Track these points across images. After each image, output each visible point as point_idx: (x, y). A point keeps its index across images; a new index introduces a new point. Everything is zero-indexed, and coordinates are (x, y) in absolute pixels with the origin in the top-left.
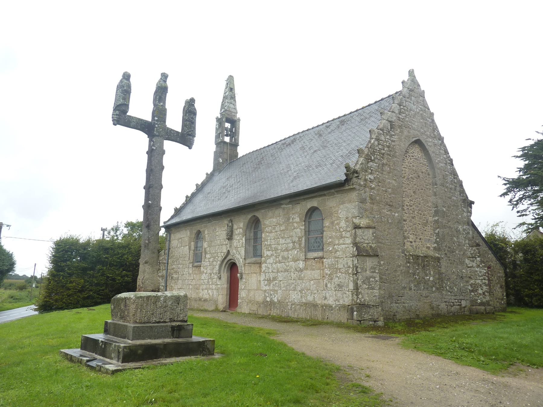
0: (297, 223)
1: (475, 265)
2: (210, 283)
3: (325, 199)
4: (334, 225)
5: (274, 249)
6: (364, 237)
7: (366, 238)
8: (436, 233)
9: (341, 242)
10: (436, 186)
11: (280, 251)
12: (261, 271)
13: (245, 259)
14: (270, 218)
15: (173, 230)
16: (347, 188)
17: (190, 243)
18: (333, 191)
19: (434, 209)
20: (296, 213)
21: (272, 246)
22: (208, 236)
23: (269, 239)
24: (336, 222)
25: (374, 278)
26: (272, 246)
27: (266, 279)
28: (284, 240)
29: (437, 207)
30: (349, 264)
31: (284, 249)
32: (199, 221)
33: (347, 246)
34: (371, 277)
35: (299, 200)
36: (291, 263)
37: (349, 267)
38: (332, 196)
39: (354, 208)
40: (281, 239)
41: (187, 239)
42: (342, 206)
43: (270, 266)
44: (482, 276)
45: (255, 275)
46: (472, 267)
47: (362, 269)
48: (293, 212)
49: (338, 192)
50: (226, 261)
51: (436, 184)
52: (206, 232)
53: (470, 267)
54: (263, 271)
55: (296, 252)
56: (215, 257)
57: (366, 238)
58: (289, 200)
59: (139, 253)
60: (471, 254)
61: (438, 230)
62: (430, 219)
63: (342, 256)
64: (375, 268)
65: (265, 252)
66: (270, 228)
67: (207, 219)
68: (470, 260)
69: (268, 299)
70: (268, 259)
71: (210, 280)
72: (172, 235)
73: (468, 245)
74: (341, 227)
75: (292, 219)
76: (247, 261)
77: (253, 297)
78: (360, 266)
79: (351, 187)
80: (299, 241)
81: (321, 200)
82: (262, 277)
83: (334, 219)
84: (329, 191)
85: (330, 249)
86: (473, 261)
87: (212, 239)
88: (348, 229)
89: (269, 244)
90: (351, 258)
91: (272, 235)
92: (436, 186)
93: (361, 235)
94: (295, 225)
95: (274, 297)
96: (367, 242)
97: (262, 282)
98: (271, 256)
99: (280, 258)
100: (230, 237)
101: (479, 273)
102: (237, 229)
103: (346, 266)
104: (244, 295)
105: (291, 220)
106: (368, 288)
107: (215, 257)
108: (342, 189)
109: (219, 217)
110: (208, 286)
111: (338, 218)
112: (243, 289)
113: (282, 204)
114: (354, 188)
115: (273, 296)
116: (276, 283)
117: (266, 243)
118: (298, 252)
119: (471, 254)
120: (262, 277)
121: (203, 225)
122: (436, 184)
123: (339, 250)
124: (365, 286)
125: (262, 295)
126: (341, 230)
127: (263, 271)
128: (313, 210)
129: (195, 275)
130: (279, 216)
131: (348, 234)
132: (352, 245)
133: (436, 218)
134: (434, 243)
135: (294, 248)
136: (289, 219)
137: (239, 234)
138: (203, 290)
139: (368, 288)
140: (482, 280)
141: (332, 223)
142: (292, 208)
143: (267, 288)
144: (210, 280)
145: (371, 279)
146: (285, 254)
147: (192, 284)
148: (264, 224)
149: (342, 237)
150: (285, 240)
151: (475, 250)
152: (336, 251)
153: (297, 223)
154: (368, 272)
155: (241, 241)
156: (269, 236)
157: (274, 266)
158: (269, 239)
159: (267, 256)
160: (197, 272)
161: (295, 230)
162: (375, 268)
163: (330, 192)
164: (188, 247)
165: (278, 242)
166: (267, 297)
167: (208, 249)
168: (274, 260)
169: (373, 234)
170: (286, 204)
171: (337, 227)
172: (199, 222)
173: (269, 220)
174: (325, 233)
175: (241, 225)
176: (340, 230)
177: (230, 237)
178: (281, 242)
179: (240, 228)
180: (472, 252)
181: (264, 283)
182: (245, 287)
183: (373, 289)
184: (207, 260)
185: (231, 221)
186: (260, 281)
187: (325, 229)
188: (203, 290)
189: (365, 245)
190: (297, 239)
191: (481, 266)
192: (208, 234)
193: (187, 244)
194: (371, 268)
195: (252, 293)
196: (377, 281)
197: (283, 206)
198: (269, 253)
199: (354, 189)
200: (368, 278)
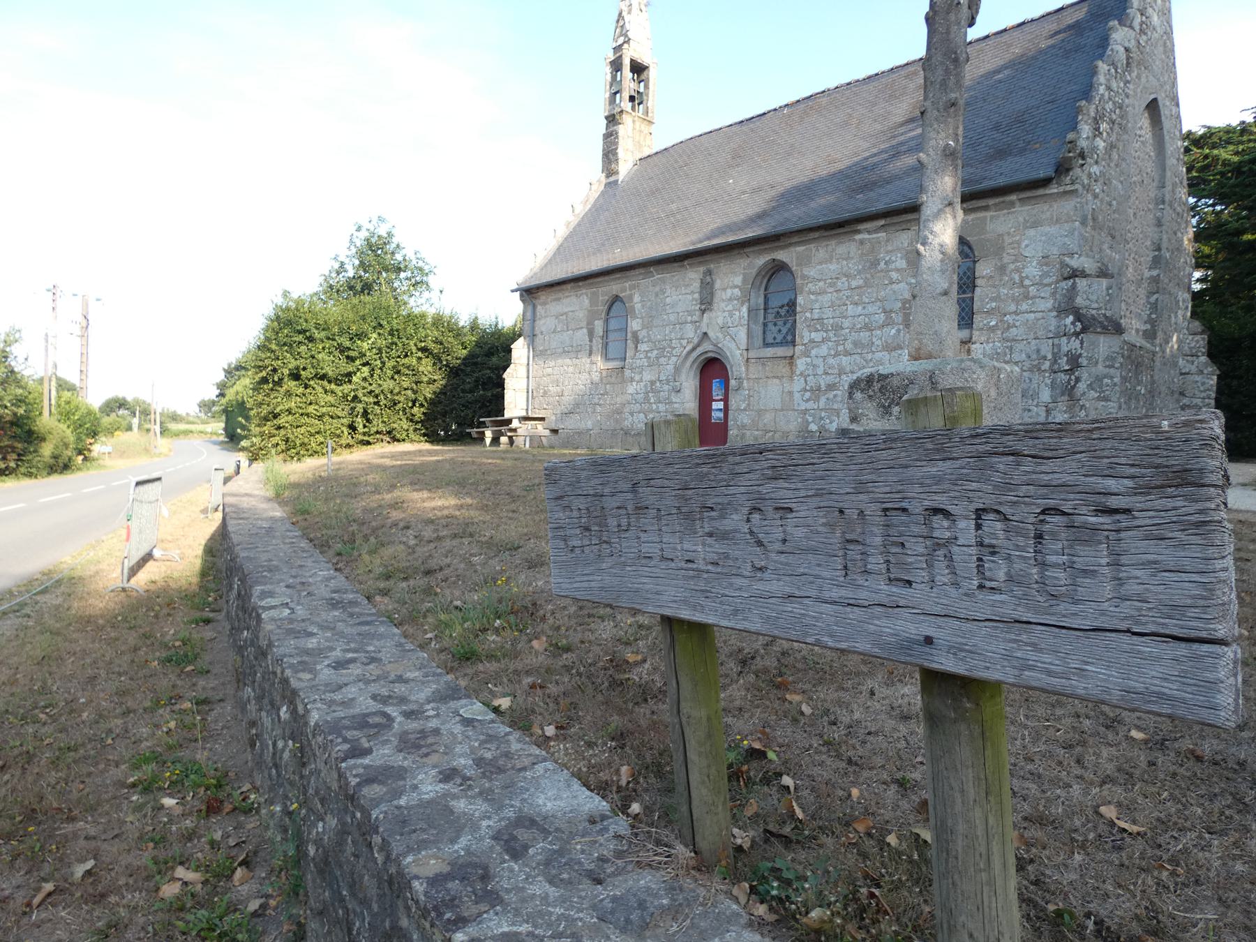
0: (898, 270)
1: (1193, 368)
2: (652, 401)
3: (986, 217)
4: (1008, 272)
5: (832, 326)
6: (1090, 297)
7: (1094, 298)
8: (1150, 303)
9: (1024, 307)
10: (1162, 206)
11: (847, 331)
12: (793, 372)
13: (747, 350)
14: (821, 263)
15: (543, 296)
16: (1056, 191)
17: (590, 324)
18: (1013, 197)
19: (1152, 254)
20: (898, 249)
21: (825, 321)
22: (643, 306)
23: (817, 306)
24: (1012, 266)
25: (1112, 378)
26: (825, 321)
27: (808, 388)
28: (860, 308)
29: (1159, 249)
30: (1043, 353)
31: (859, 326)
32: (618, 276)
33: (1039, 315)
34: (1106, 376)
35: (909, 221)
36: (880, 354)
37: (1045, 358)
38: (1005, 211)
39: (1066, 236)
40: (850, 307)
41: (581, 314)
42: (1032, 232)
43: (819, 362)
44: (1205, 391)
45: (777, 381)
46: (1188, 374)
47: (1090, 359)
48: (890, 248)
49: (998, 207)
50: (695, 354)
51: (1163, 202)
52: (637, 298)
53: (1185, 374)
54: (798, 373)
55: (893, 331)
56: (664, 348)
57: (1094, 298)
58: (882, 222)
59: (268, 381)
60: (1191, 348)
61: (1155, 296)
62: (1147, 274)
63: (1025, 337)
64: (1113, 359)
65: (806, 334)
66: (821, 284)
67: (642, 271)
68: (1187, 361)
69: (813, 427)
70: (813, 348)
71: (650, 395)
72: (539, 307)
73: (1186, 331)
74: (1027, 277)
75: (886, 263)
76: (752, 354)
77: (773, 424)
78: (1085, 354)
79: (1069, 188)
80: (904, 308)
81: (973, 220)
82: (798, 384)
83: (1006, 259)
84: (1001, 199)
85: (993, 323)
86: (1193, 363)
87: (654, 313)
88: (1046, 281)
89: (816, 317)
90: (1051, 341)
91: (826, 299)
92: (1162, 206)
93: (1085, 292)
94: (894, 275)
95: (831, 423)
96: (1095, 305)
97: (797, 396)
98: (823, 341)
99: (849, 346)
100: (706, 303)
101: (1199, 384)
102: (724, 289)
103: (1034, 356)
104: (745, 421)
105: (882, 264)
106: (1099, 399)
107: (664, 348)
108: (1041, 192)
109: (676, 265)
110: (646, 407)
111: (1019, 257)
112: (745, 410)
113: (859, 232)
114: (1074, 192)
115: (828, 421)
116: (835, 396)
117: (808, 315)
118: (899, 331)
119: (1191, 348)
120: (798, 384)
121: (627, 285)
122: (1163, 202)
123: (1018, 324)
124: (1093, 394)
125: (796, 420)
126: (1027, 282)
127: (798, 373)
128: (616, 299)
129: (608, 386)
130: (848, 259)
131: (1046, 292)
132: (1055, 313)
133: (1155, 273)
134: (1146, 323)
135: (888, 323)
136: (875, 263)
137: (730, 299)
138: (632, 414)
139: (1099, 399)
140: (1204, 398)
141: (1002, 269)
142: (888, 241)
143: (811, 405)
144: (650, 395)
145: (1106, 380)
146: (864, 335)
147: (601, 402)
148: (804, 277)
149: (1026, 297)
150: (864, 308)
151: (1197, 342)
152: (1009, 327)
153: (898, 270)
154: (1100, 367)
155: (737, 313)
156: (817, 301)
157: (831, 361)
158: (817, 306)
159: (812, 341)
160: (613, 380)
161: (893, 286)
162: (1113, 359)
163: (1003, 202)
164: (585, 331)
165: (841, 313)
166: (808, 423)
167: (643, 334)
168: (829, 349)
169: (1108, 289)
170: (869, 232)
171: (1016, 277)
172: (619, 278)
173: (819, 267)
174: (978, 290)
175: (738, 280)
176: (1022, 282)
177: (706, 303)
178: (850, 313)
179: (736, 287)
180: (1192, 345)
181: (803, 396)
182: (749, 405)
183: (1106, 399)
184: (642, 356)
185: (709, 273)
186: (791, 393)
187: (978, 282)
188: (632, 414)
189: (1094, 312)
190: (900, 305)
191: (1205, 372)
192: (642, 301)
193: (584, 324)
194: (1107, 358)
195: (768, 418)
196: (1115, 385)
197: (858, 237)
198: (817, 336)
199: (1074, 192)
200: (1099, 379)
